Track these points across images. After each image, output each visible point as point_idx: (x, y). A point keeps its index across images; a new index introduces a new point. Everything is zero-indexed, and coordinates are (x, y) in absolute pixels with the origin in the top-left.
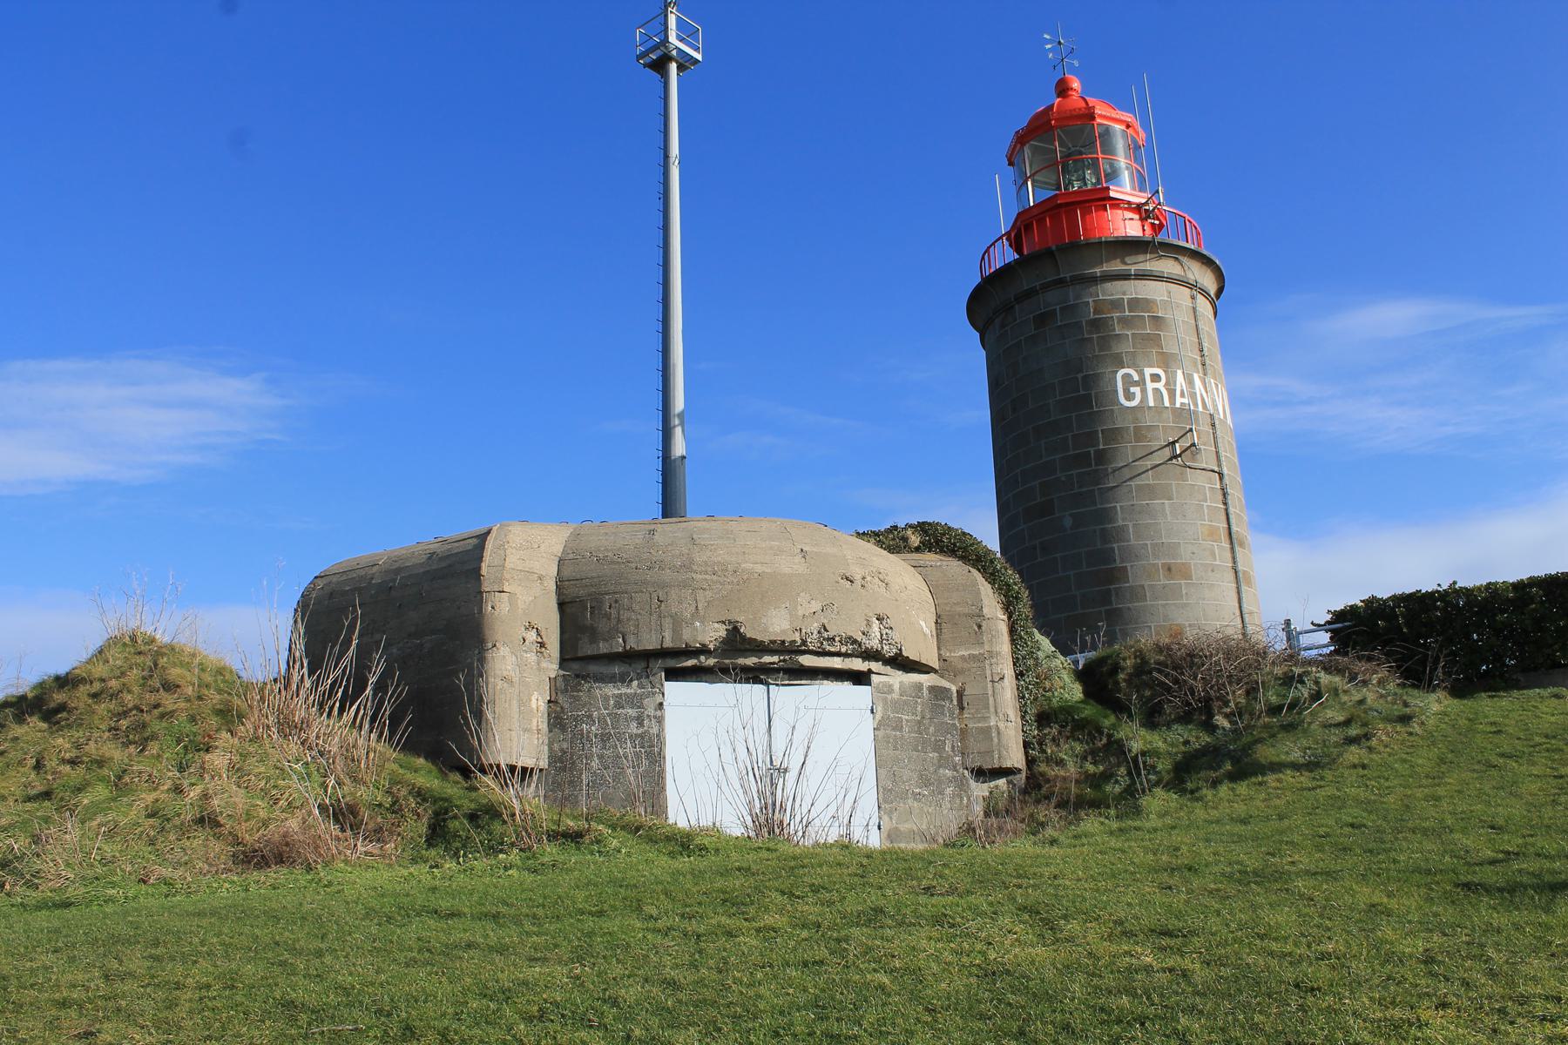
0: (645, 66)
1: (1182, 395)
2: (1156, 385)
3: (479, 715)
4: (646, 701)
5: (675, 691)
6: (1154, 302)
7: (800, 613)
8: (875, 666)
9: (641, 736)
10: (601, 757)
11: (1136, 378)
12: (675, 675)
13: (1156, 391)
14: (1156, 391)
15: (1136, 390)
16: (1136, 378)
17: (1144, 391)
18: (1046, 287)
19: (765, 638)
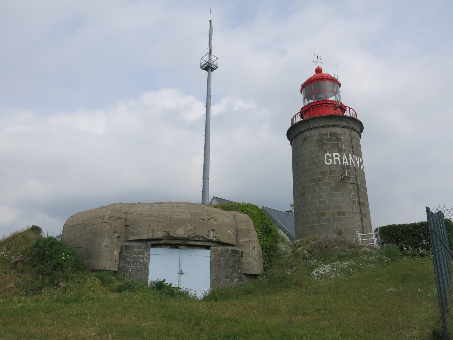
1: (345, 161)
2: (337, 158)
3: (171, 248)
4: (145, 253)
5: (154, 251)
6: (337, 133)
7: (188, 229)
8: (212, 244)
9: (143, 263)
10: (132, 268)
11: (330, 156)
12: (153, 246)
13: (337, 160)
14: (337, 160)
16: (330, 156)
17: (333, 160)
18: (306, 131)
19: (175, 236)
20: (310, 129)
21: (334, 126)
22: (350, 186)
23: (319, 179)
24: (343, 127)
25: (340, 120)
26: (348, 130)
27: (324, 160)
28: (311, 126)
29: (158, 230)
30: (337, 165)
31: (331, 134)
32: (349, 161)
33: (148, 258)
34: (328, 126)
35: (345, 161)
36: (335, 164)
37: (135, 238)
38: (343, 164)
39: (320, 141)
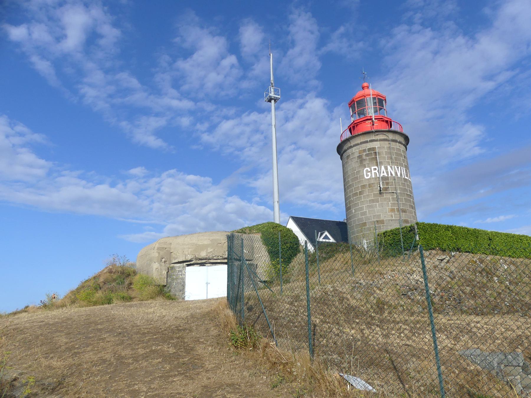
1: (383, 173)
11: (369, 170)
12: (188, 265)
13: (375, 173)
14: (375, 173)
16: (369, 170)
17: (371, 174)
19: (200, 257)
20: (351, 147)
21: (372, 141)
22: (389, 196)
23: (361, 193)
24: (381, 140)
25: (377, 135)
28: (352, 145)
29: (188, 254)
31: (370, 149)
32: (387, 173)
33: (185, 275)
35: (383, 173)
36: (373, 177)
37: (177, 261)
39: (360, 157)
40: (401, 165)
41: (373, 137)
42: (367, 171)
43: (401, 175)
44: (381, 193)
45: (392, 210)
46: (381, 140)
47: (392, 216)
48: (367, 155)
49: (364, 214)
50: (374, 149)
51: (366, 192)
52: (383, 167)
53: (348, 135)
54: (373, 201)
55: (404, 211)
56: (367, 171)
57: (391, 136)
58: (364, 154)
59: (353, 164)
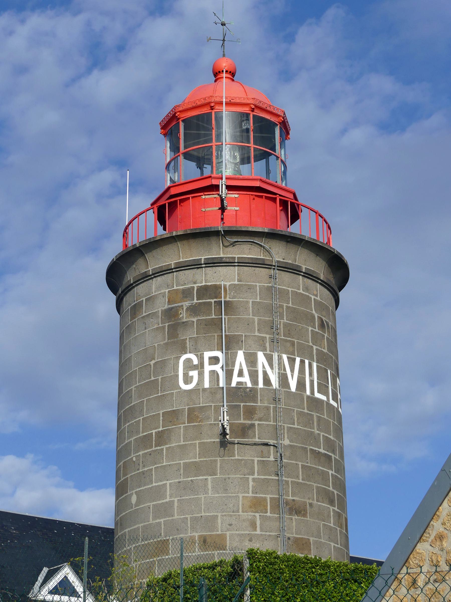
0: (275, 152)
1: (241, 374)
2: (213, 367)
11: (196, 361)
13: (213, 374)
14: (213, 374)
15: (194, 374)
16: (196, 361)
17: (201, 374)
20: (146, 277)
21: (213, 263)
22: (251, 456)
23: (162, 438)
24: (242, 263)
25: (233, 244)
26: (263, 272)
27: (177, 376)
30: (215, 390)
31: (204, 291)
32: (254, 375)
34: (196, 265)
35: (241, 374)
36: (207, 385)
38: (234, 384)
39: (171, 314)
40: (305, 352)
41: (218, 251)
42: (189, 365)
43: (301, 384)
44: (224, 443)
45: (257, 505)
46: (242, 263)
47: (253, 525)
48: (193, 310)
49: (165, 510)
50: (211, 291)
51: (180, 434)
52: (240, 357)
53: (149, 228)
54: (196, 468)
55: (297, 510)
56: (189, 365)
57: (279, 253)
58: (186, 304)
59: (150, 335)
